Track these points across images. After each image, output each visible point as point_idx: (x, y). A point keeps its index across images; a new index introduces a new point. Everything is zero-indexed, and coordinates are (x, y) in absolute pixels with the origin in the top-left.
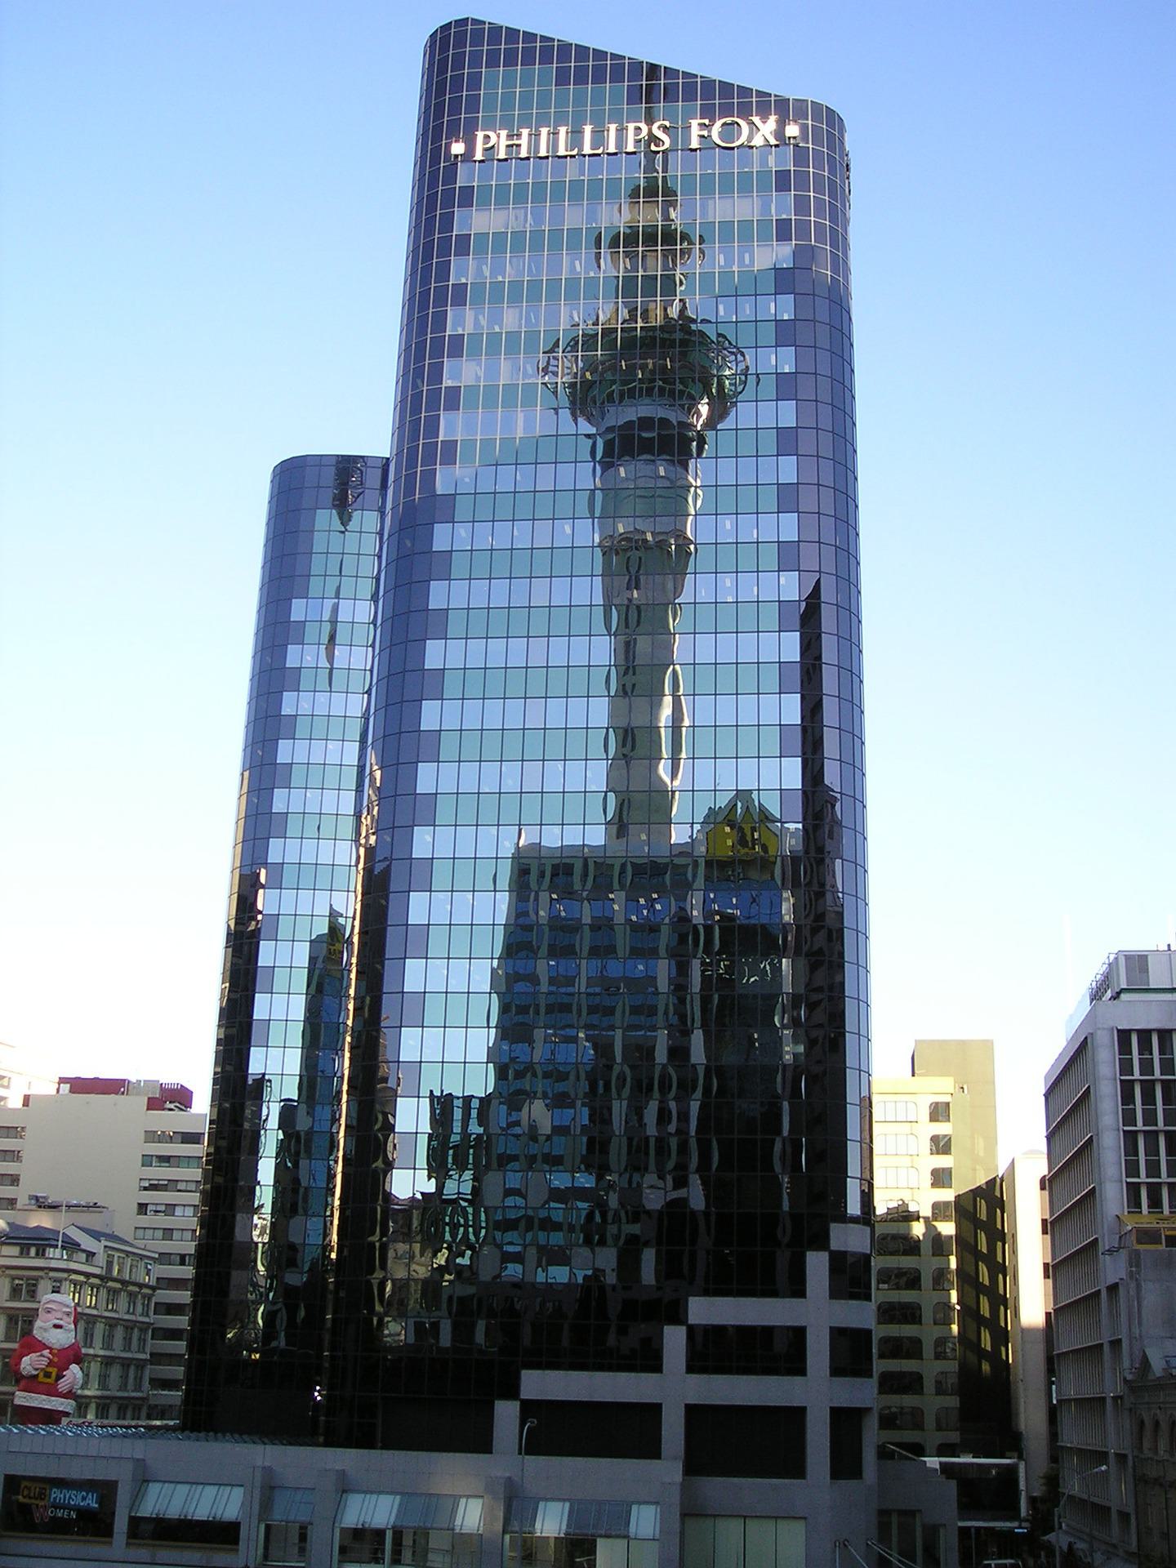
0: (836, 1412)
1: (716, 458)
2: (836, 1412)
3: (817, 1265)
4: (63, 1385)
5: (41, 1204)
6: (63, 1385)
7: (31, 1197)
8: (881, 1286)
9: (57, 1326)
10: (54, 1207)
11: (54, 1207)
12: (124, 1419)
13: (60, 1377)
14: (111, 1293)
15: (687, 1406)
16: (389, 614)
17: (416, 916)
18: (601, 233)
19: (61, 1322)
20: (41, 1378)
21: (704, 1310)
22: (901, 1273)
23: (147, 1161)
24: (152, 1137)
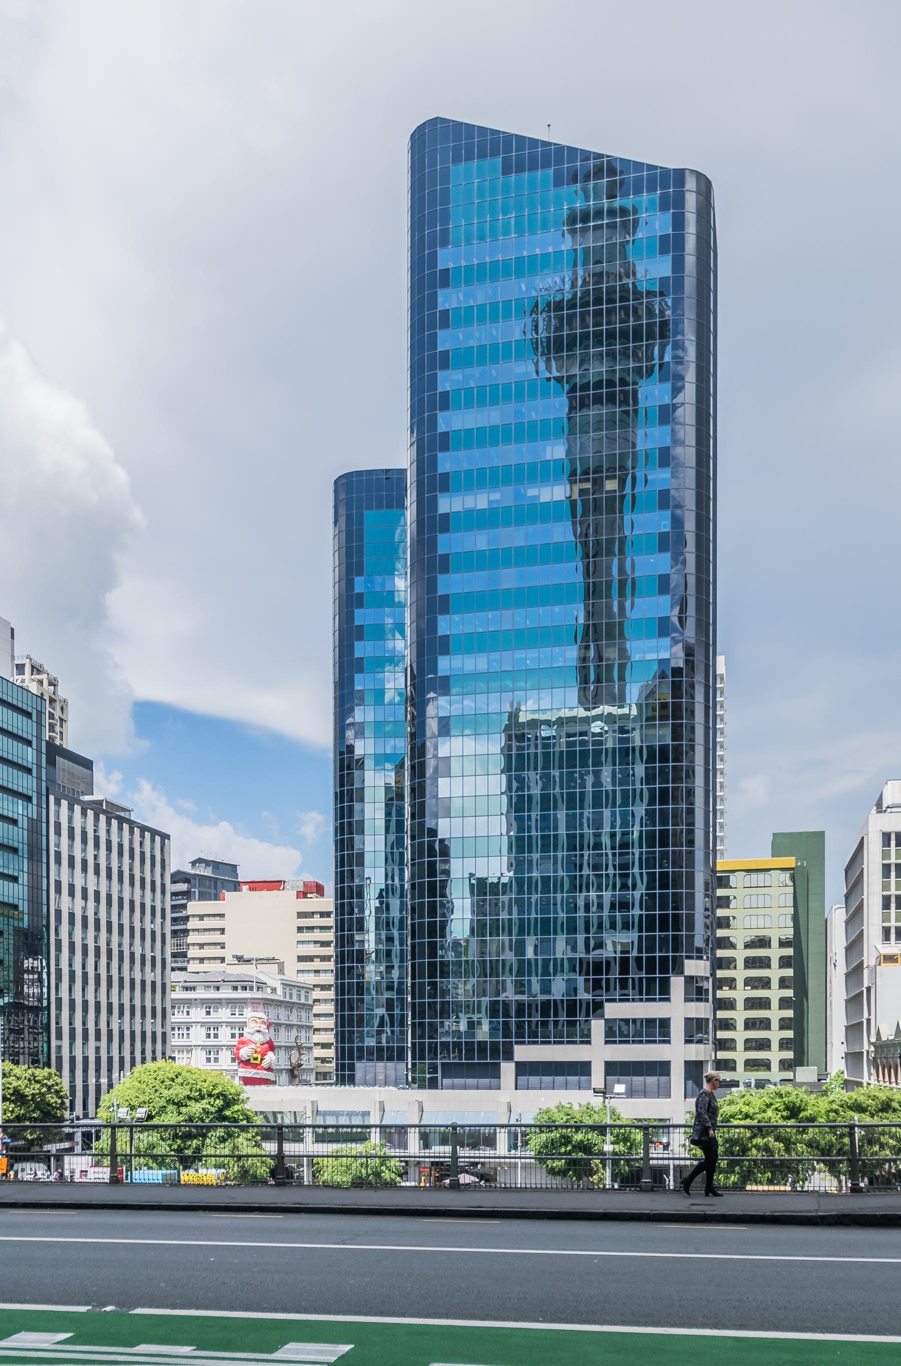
0: (688, 1064)
1: (463, 817)
2: (688, 1064)
3: (677, 984)
4: (265, 1064)
5: (240, 959)
6: (265, 1064)
7: (234, 956)
8: (746, 988)
9: (259, 1031)
10: (248, 961)
11: (248, 961)
12: (326, 1080)
13: (262, 1060)
14: (90, 813)
15: (606, 1062)
16: (415, 599)
17: (443, 792)
18: (537, 302)
19: (260, 1029)
20: (252, 1061)
21: (614, 1010)
22: (760, 979)
23: (300, 929)
24: (301, 915)
